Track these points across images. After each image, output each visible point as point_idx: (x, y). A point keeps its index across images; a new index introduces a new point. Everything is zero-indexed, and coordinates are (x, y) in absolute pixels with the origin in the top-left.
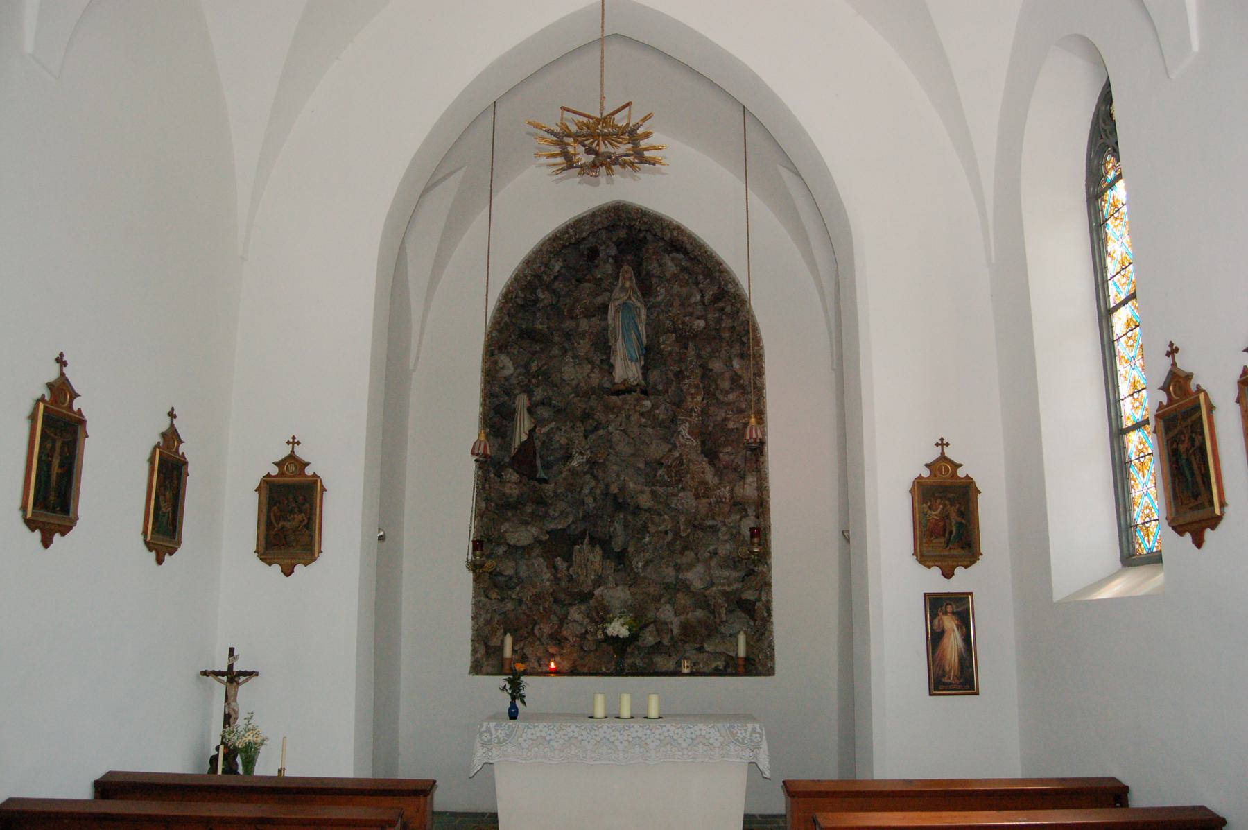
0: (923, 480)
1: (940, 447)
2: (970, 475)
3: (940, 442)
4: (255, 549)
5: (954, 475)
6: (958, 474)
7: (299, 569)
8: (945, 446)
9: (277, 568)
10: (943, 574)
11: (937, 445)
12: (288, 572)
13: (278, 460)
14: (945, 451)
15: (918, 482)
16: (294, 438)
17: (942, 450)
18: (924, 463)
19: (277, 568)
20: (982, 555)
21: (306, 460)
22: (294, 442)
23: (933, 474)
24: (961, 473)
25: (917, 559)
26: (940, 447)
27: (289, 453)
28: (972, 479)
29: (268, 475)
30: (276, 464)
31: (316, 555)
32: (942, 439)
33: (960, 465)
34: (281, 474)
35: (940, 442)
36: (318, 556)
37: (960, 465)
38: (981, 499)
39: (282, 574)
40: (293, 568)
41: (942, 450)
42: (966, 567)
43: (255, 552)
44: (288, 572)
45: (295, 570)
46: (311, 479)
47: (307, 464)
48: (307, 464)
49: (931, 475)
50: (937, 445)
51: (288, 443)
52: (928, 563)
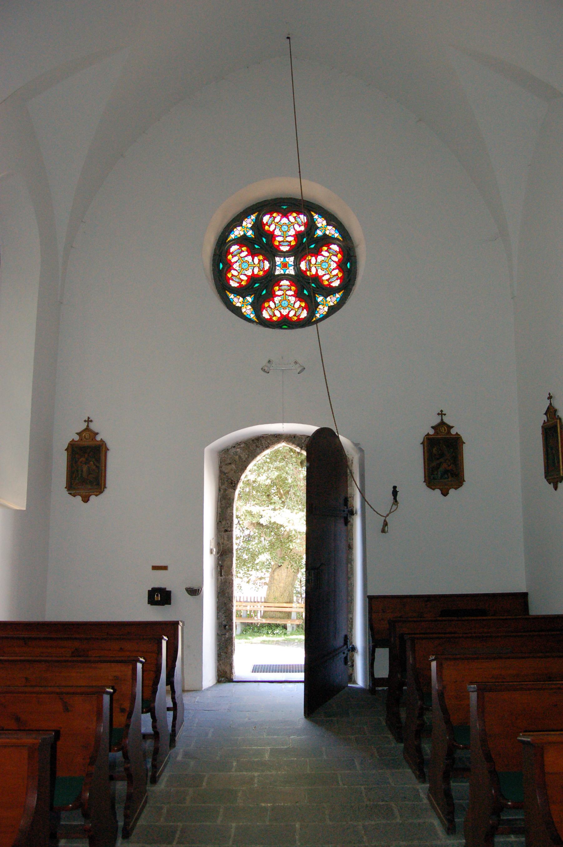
0: (431, 437)
1: (440, 415)
2: (458, 433)
3: (440, 413)
4: (424, 480)
5: (449, 432)
6: (452, 433)
7: (93, 498)
8: (90, 423)
9: (79, 498)
10: (442, 493)
11: (438, 414)
12: (445, 494)
13: (434, 425)
14: (443, 418)
15: (427, 438)
16: (89, 418)
17: (88, 424)
18: (431, 426)
19: (438, 492)
20: (465, 481)
21: (96, 431)
22: (89, 421)
23: (436, 433)
24: (453, 432)
25: (426, 485)
26: (440, 415)
27: (86, 427)
28: (460, 435)
29: (428, 434)
30: (77, 434)
31: (103, 489)
32: (442, 411)
33: (452, 427)
34: (81, 439)
35: (440, 413)
36: (104, 490)
37: (452, 427)
38: (110, 455)
39: (82, 501)
40: (89, 498)
41: (88, 424)
42: (97, 495)
43: (424, 482)
44: (445, 494)
45: (90, 499)
46: (455, 436)
47: (97, 434)
48: (97, 434)
49: (435, 433)
50: (438, 414)
51: (85, 421)
52: (432, 487)
